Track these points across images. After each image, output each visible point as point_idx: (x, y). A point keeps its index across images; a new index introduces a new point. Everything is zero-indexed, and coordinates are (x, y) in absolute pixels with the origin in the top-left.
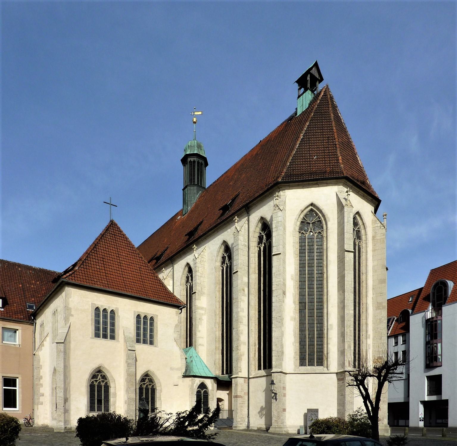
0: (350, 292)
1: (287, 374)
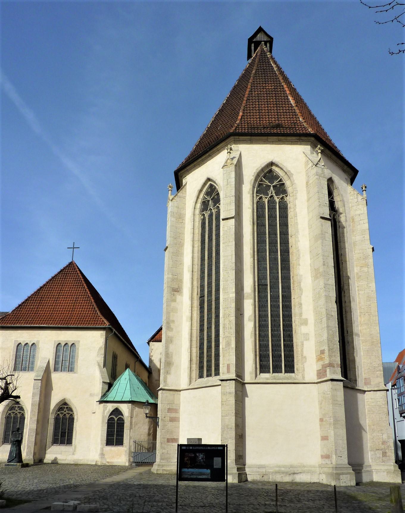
0: (229, 270)
1: (180, 391)
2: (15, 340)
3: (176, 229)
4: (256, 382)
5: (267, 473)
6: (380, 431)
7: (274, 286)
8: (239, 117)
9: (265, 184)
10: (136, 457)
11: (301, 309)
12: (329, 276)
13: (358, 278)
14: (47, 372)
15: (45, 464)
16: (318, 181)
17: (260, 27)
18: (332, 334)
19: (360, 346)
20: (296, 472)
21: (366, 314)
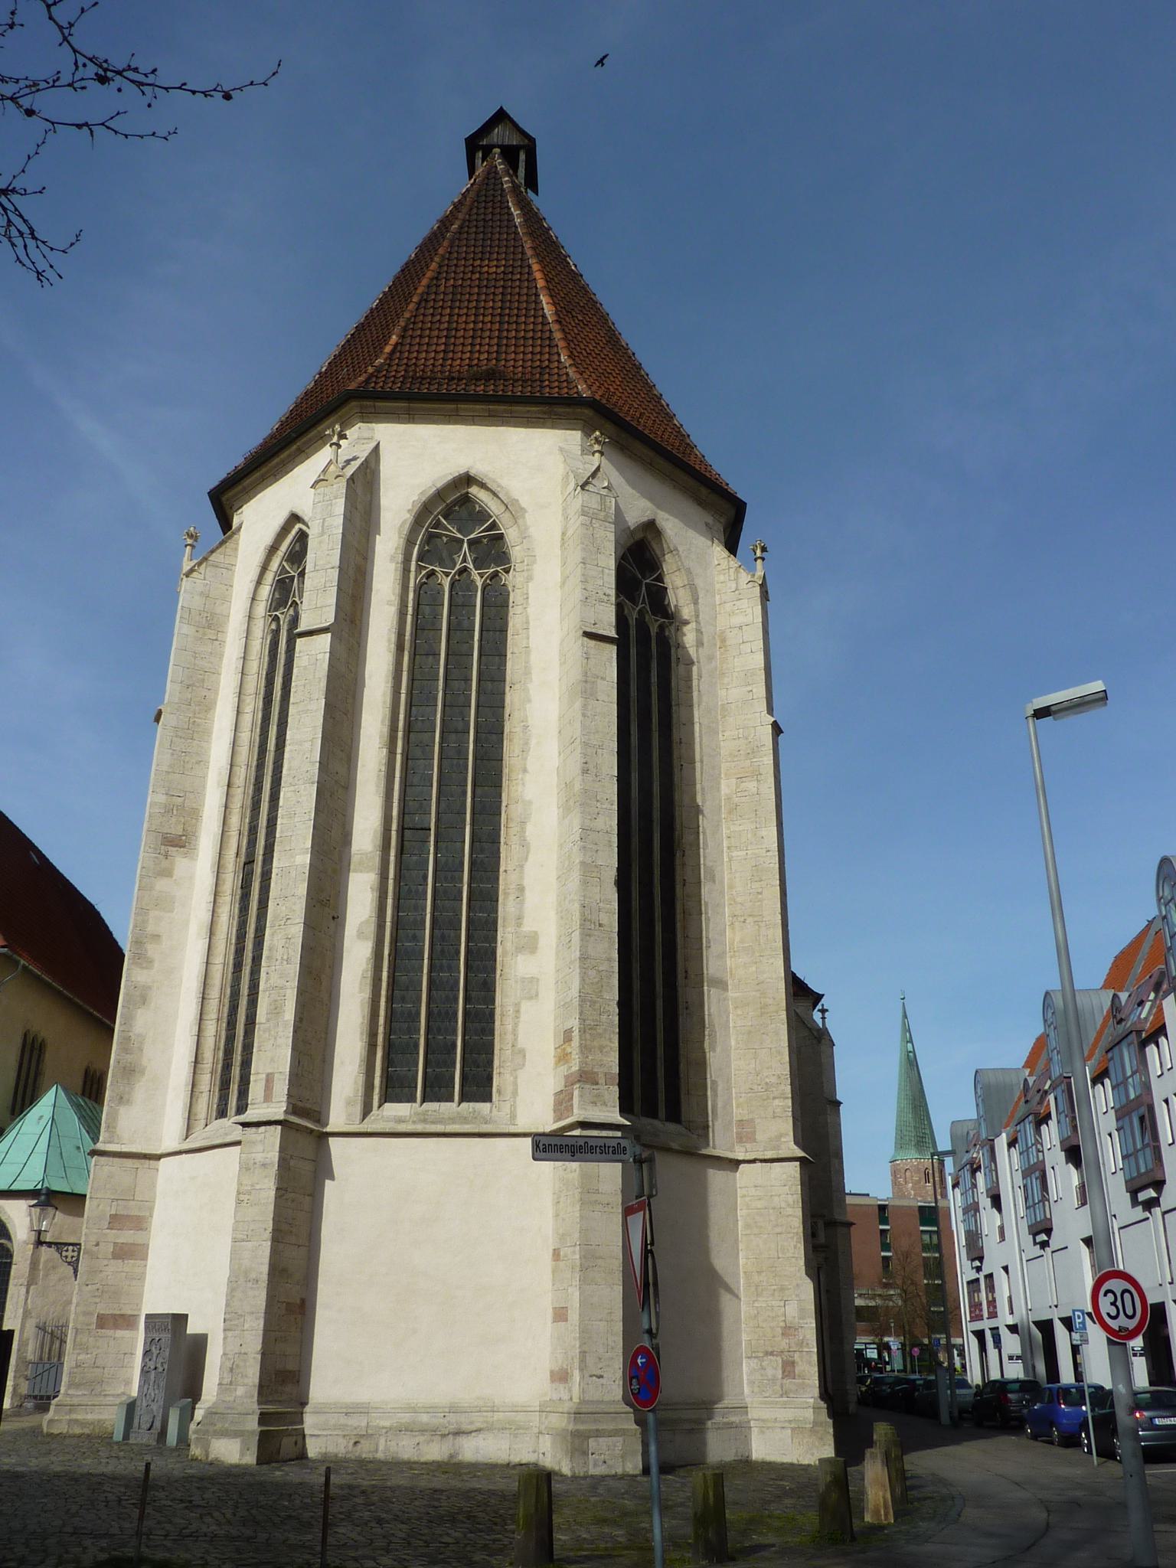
4: (362, 1130)
5: (370, 1432)
6: (776, 1293)
7: (448, 834)
8: (388, 349)
9: (447, 536)
10: (39, 1378)
11: (522, 903)
13: (730, 812)
16: (586, 532)
17: (501, 108)
18: (596, 980)
19: (728, 1017)
20: (465, 1427)
21: (750, 920)
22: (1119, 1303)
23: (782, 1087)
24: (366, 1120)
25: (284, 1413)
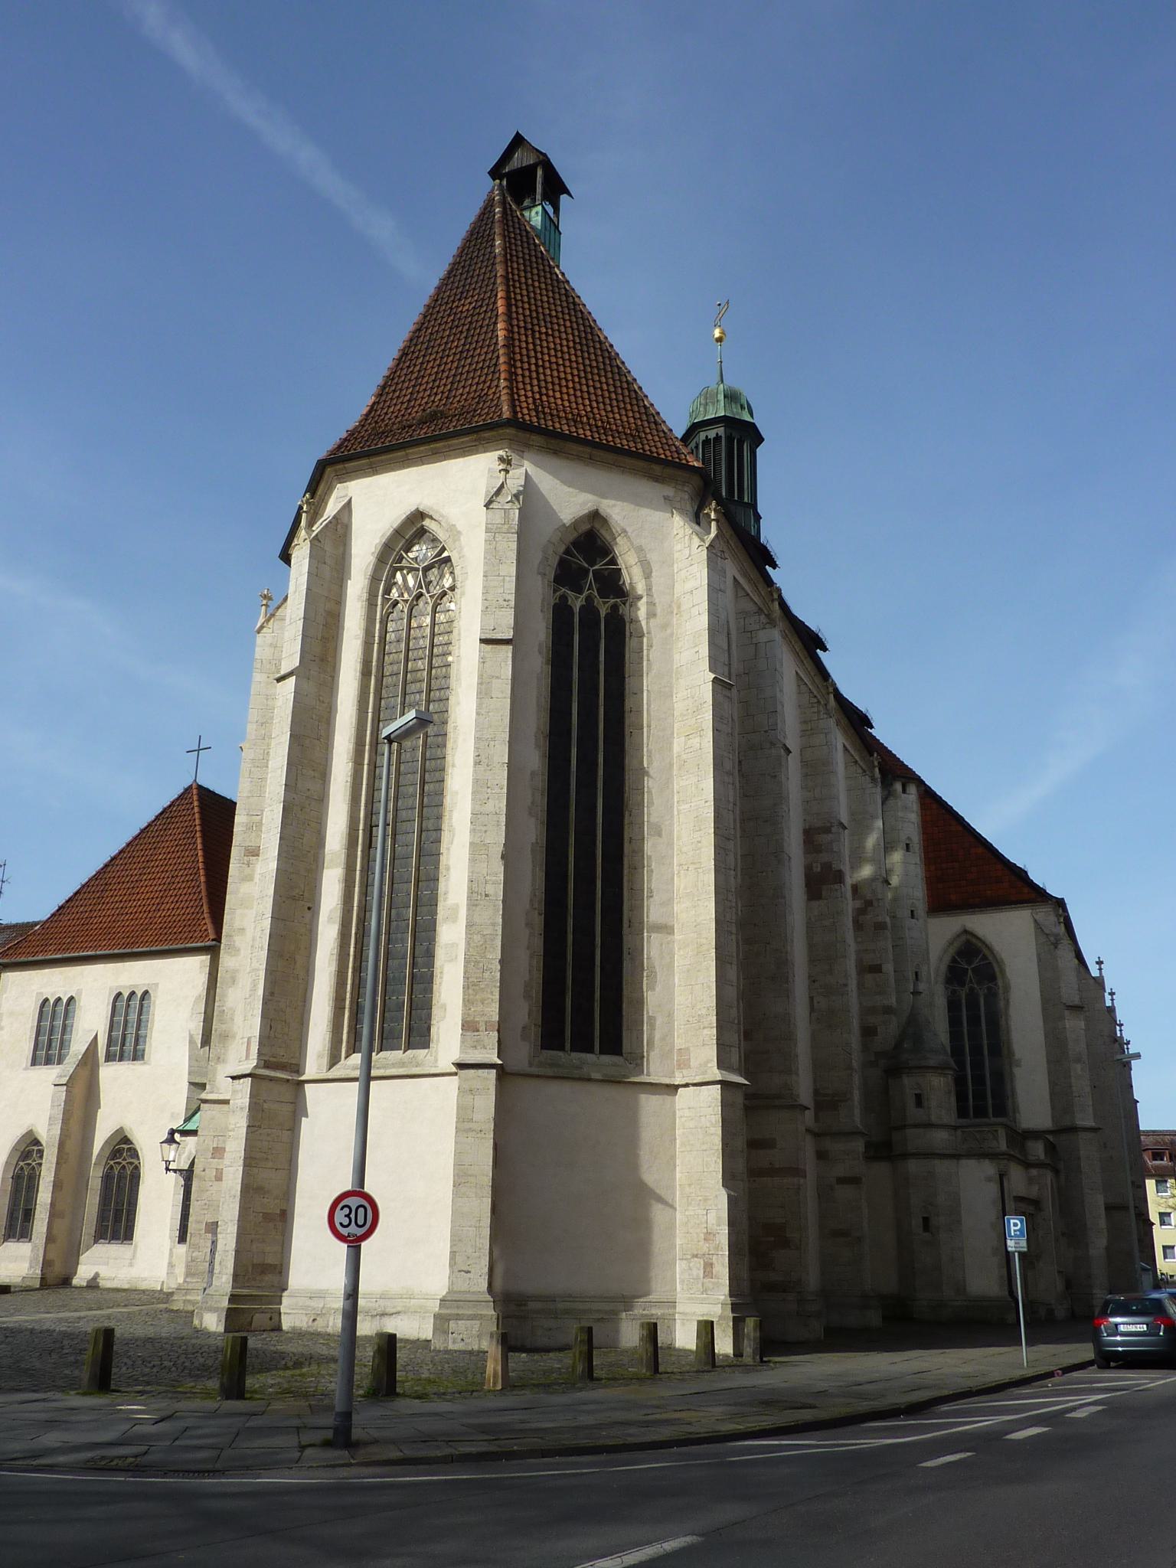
2: (37, 993)
3: (267, 699)
5: (324, 1312)
12: (489, 790)
14: (89, 1060)
15: (76, 1287)
17: (518, 132)
18: (481, 943)
21: (692, 867)
22: (353, 1216)
23: (709, 1018)
24: (331, 1070)
25: (263, 1296)
